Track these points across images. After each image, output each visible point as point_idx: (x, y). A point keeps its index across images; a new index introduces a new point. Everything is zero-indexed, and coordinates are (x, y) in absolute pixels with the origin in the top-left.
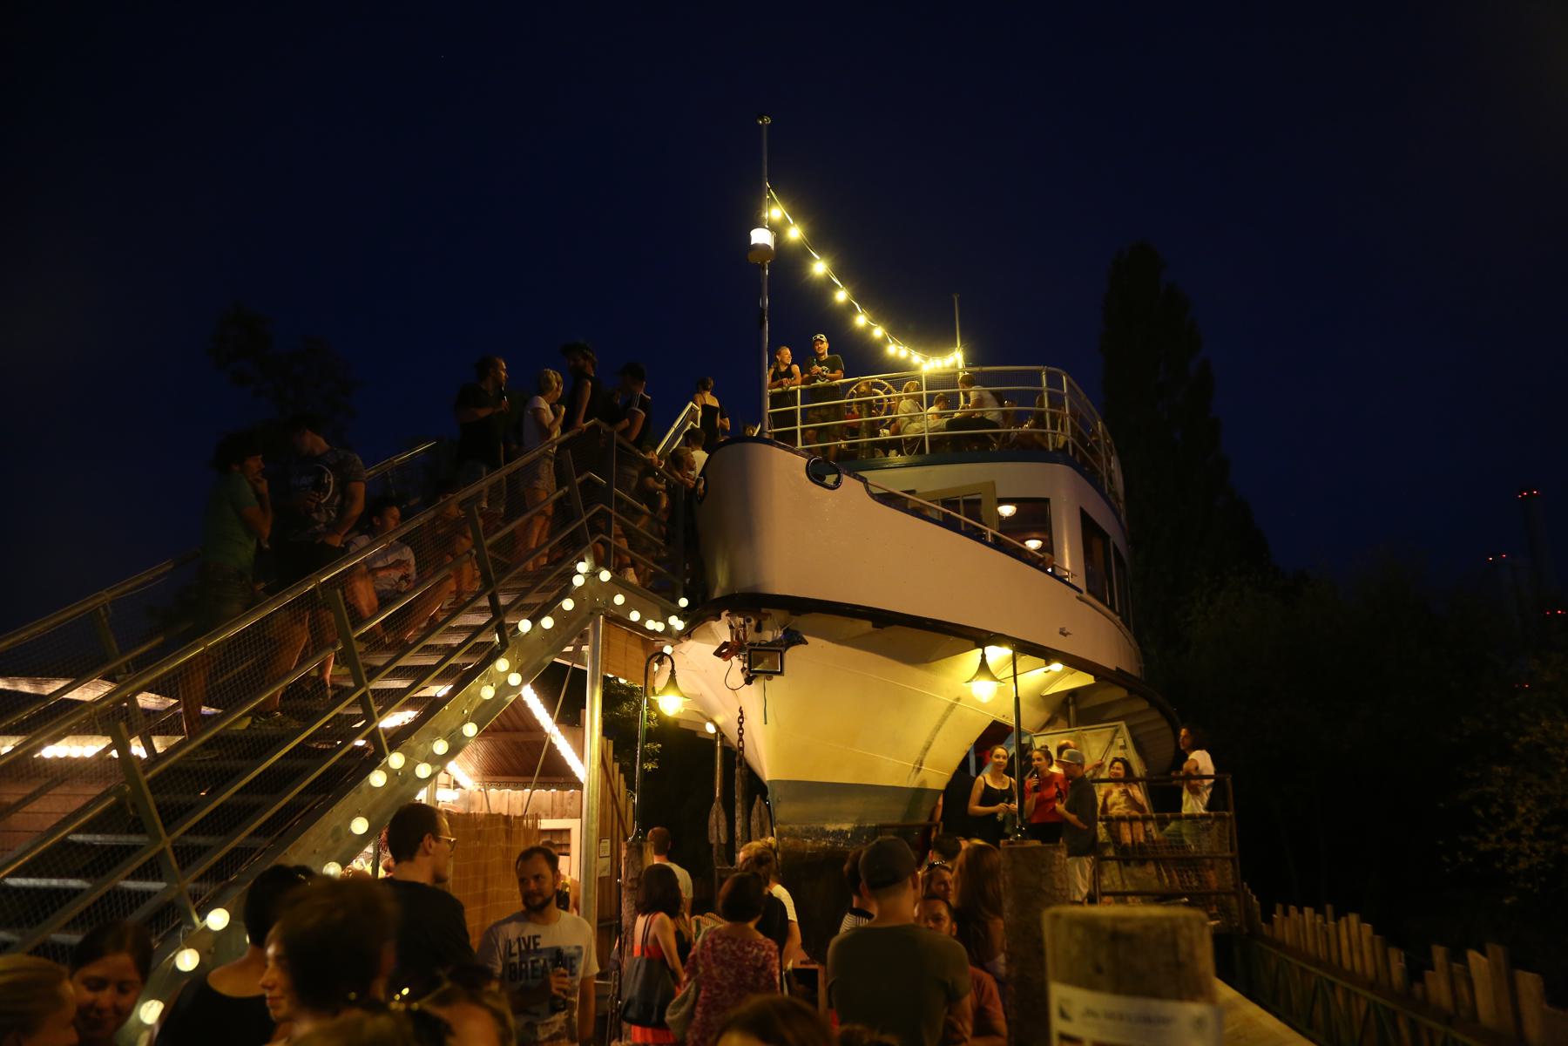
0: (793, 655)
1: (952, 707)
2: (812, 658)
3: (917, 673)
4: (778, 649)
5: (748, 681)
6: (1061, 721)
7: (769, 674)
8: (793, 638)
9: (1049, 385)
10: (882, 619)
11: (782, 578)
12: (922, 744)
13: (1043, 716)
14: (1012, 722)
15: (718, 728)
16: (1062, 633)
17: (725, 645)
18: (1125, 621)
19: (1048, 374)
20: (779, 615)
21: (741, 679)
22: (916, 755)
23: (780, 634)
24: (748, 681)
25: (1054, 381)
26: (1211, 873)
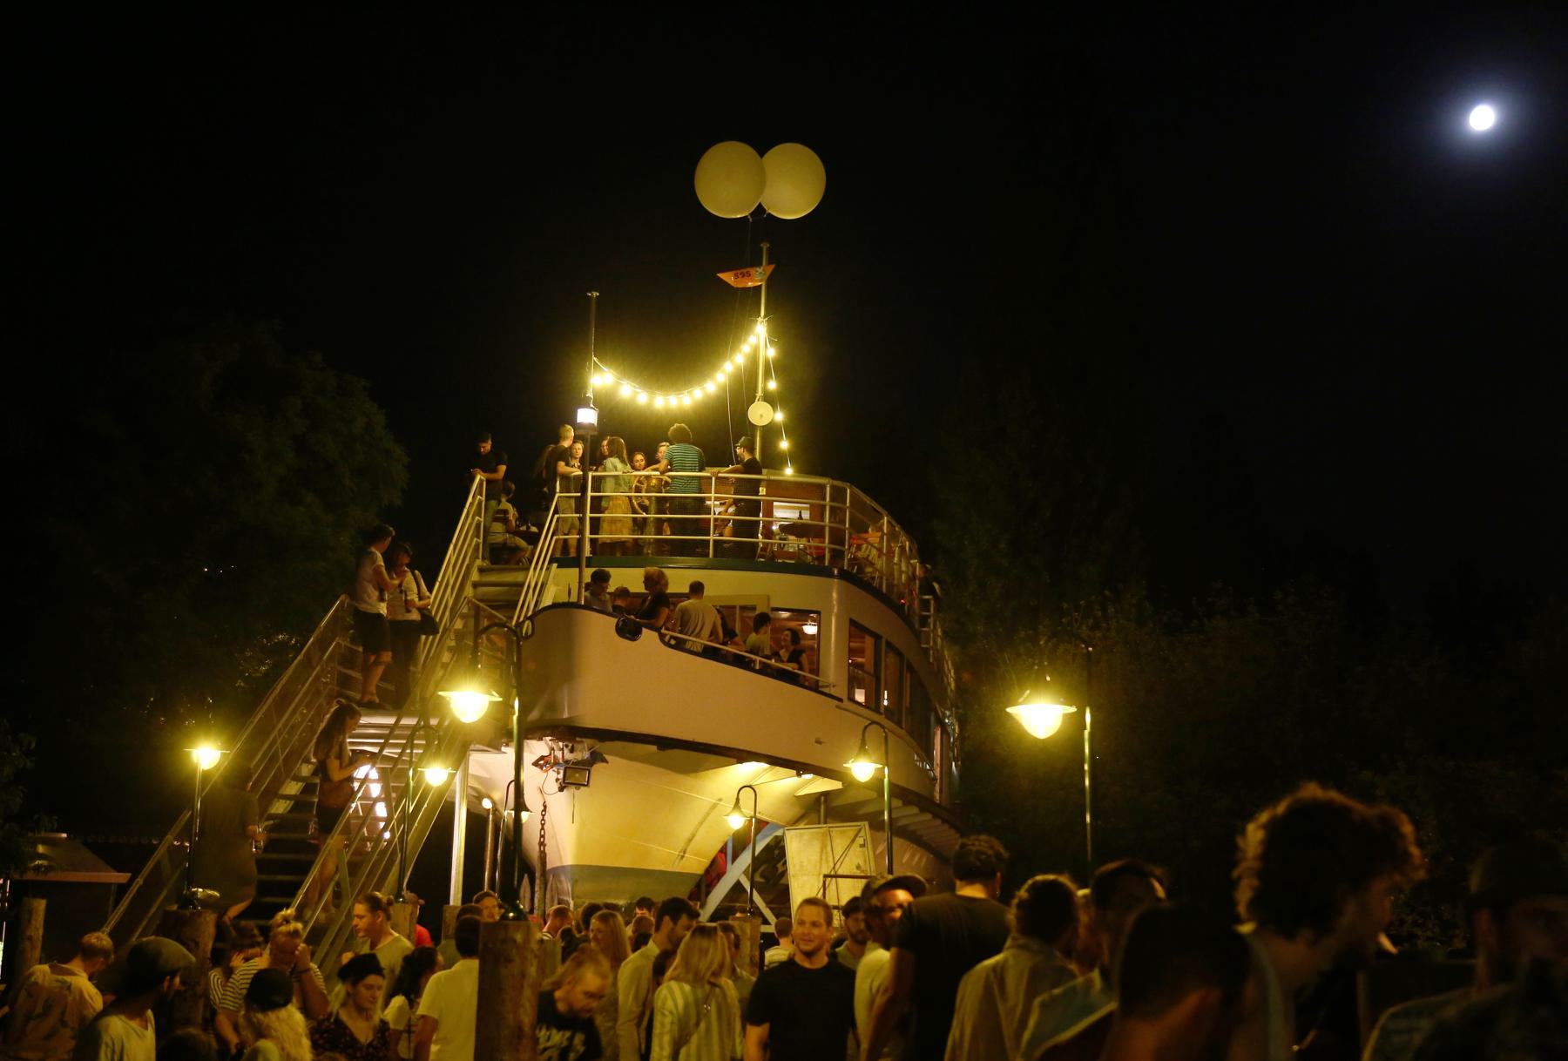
0: (598, 768)
1: (715, 806)
2: (613, 772)
3: (689, 780)
4: (585, 766)
5: (561, 789)
6: (814, 816)
7: (578, 785)
8: (596, 758)
9: (832, 499)
10: (664, 743)
11: (591, 717)
12: (687, 835)
13: (796, 811)
14: (864, 881)
15: (494, 803)
16: (818, 742)
17: (542, 758)
18: (911, 734)
19: (833, 487)
20: (587, 742)
21: (556, 786)
22: (681, 845)
23: (586, 755)
24: (561, 789)
25: (838, 495)
26: (778, 513)
